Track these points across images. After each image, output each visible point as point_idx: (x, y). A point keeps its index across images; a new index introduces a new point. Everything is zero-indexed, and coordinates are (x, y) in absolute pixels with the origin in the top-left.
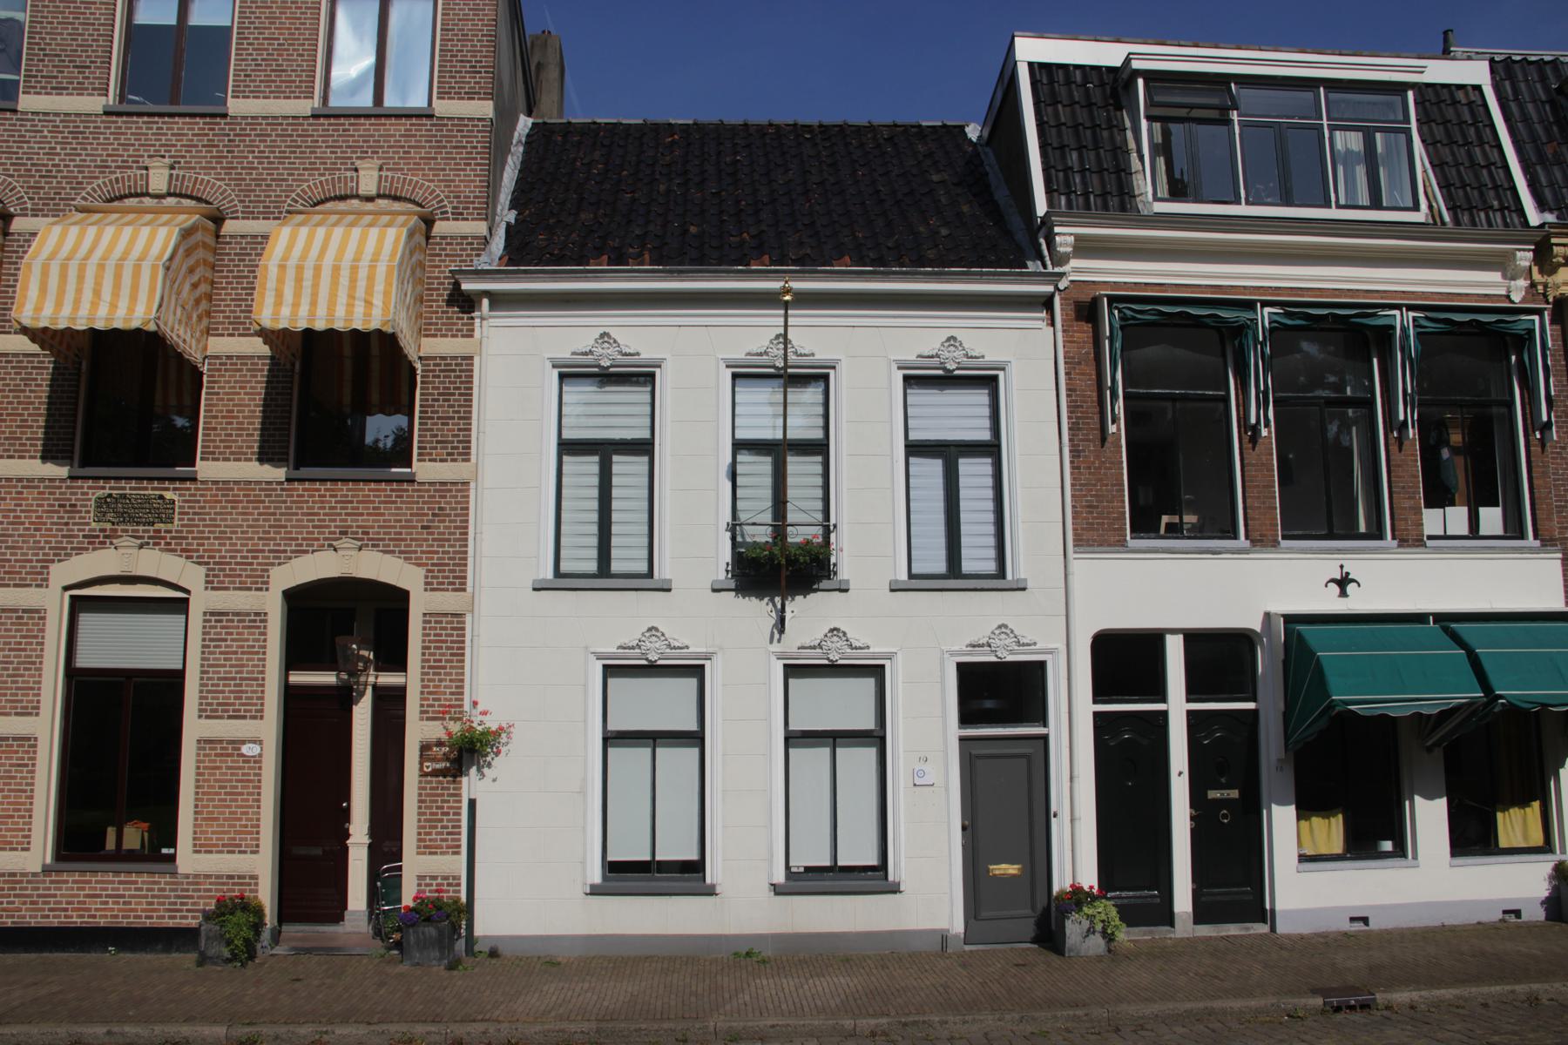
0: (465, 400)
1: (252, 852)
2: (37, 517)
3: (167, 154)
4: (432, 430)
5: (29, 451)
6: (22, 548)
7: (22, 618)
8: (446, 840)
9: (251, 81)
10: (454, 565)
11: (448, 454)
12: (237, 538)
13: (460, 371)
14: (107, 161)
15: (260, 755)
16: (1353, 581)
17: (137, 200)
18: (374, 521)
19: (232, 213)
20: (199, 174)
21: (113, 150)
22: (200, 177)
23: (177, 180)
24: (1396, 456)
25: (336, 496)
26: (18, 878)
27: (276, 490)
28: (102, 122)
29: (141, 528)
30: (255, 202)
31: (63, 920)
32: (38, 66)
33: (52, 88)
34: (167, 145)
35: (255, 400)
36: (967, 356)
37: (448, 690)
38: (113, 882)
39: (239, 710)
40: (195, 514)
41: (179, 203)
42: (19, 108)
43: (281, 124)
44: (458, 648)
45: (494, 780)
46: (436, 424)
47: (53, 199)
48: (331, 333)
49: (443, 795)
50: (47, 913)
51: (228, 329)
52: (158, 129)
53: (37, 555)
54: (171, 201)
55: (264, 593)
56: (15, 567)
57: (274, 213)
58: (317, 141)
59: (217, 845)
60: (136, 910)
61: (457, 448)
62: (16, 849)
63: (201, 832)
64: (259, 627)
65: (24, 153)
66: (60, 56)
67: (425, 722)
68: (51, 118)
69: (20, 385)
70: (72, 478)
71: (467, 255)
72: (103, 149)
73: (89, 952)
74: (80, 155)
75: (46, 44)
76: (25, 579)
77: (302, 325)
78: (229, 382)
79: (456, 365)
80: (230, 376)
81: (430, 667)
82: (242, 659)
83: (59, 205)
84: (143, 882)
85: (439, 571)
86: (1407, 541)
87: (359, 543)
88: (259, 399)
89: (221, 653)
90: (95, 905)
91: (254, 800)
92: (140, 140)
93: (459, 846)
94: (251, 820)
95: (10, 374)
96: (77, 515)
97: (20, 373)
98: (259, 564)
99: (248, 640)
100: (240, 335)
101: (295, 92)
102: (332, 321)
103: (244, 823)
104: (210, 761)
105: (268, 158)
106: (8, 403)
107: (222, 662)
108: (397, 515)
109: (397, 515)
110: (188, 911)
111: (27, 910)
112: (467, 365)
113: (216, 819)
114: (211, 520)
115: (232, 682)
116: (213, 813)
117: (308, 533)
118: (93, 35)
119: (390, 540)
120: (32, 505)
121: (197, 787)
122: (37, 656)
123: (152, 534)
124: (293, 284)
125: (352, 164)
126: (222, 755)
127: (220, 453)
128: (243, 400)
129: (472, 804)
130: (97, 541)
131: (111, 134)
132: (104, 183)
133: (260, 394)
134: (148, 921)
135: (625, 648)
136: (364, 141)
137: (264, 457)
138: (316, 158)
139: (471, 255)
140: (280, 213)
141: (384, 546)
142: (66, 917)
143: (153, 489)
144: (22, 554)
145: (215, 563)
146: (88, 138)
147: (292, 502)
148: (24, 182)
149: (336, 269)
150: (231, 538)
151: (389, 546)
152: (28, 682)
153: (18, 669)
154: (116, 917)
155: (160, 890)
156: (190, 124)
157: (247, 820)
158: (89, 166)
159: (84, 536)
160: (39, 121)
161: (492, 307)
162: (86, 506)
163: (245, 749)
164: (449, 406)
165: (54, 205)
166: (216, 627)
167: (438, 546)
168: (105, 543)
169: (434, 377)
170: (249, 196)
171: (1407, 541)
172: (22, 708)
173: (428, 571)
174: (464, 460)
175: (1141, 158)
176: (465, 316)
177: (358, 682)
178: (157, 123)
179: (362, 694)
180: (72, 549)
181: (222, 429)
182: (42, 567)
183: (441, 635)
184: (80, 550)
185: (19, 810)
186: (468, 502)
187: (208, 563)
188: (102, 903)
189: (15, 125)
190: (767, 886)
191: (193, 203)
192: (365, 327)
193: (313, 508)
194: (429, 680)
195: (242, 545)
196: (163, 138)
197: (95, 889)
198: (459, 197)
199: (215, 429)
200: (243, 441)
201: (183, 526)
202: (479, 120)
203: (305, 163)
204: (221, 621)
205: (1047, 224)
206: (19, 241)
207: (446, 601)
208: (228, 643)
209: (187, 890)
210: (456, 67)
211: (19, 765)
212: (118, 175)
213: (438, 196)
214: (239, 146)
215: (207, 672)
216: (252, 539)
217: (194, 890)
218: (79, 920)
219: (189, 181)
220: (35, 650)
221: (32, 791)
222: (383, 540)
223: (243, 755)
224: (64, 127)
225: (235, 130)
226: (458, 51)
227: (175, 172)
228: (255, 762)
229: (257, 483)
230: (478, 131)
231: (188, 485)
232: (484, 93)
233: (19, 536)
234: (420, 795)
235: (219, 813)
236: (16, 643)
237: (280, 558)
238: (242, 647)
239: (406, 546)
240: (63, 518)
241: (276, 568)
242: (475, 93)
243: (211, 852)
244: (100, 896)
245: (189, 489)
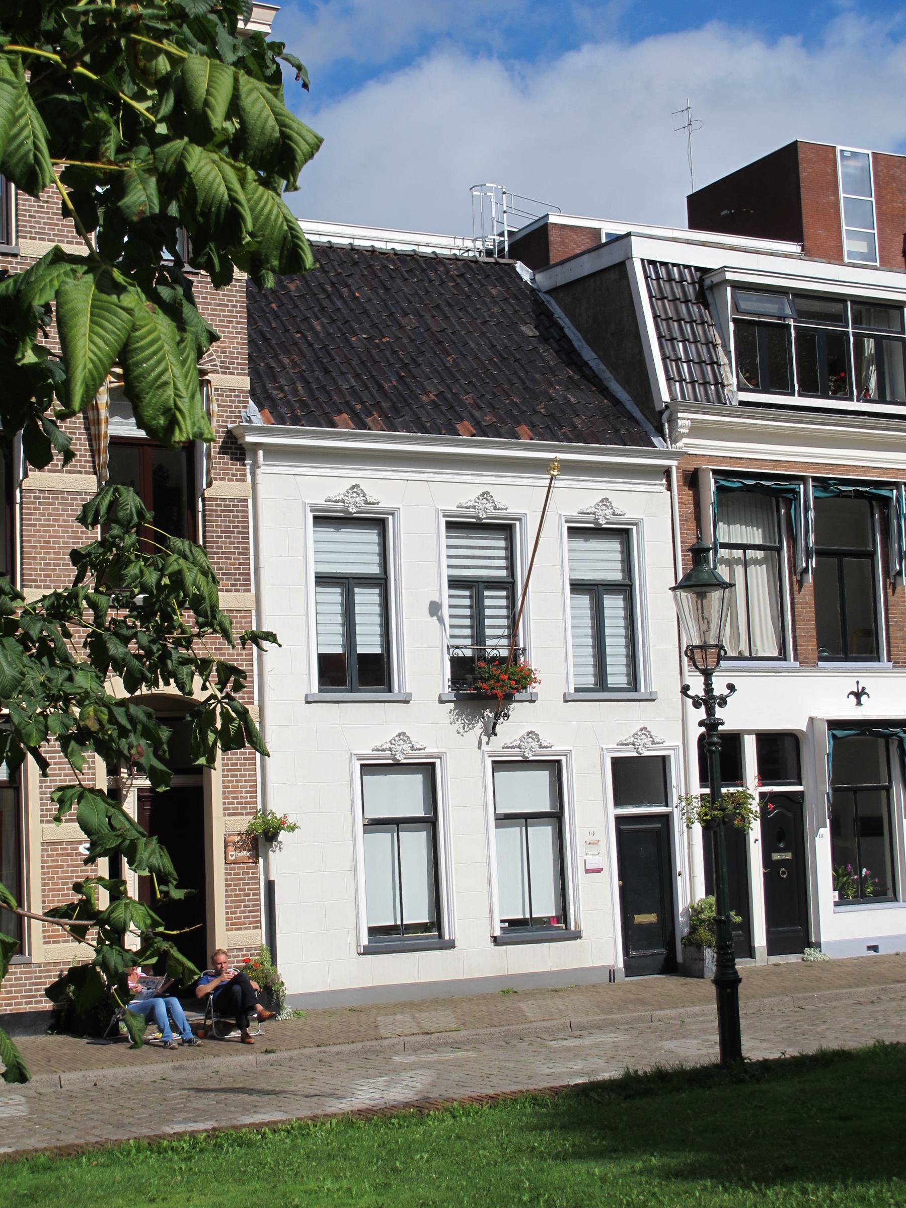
8: (248, 917)
11: (232, 585)
16: (866, 693)
24: (890, 598)
36: (366, 502)
46: (221, 558)
61: (239, 580)
67: (227, 818)
71: (236, 407)
78: (44, 515)
81: (229, 770)
86: (898, 663)
104: (53, 861)
126: (62, 855)
127: (41, 581)
128: (58, 531)
129: (270, 886)
139: (238, 407)
164: (231, 543)
169: (217, 516)
171: (898, 663)
175: (728, 354)
181: (41, 559)
190: (489, 939)
199: (35, 558)
200: (60, 570)
205: (671, 409)
209: (40, 978)
243: (58, 942)
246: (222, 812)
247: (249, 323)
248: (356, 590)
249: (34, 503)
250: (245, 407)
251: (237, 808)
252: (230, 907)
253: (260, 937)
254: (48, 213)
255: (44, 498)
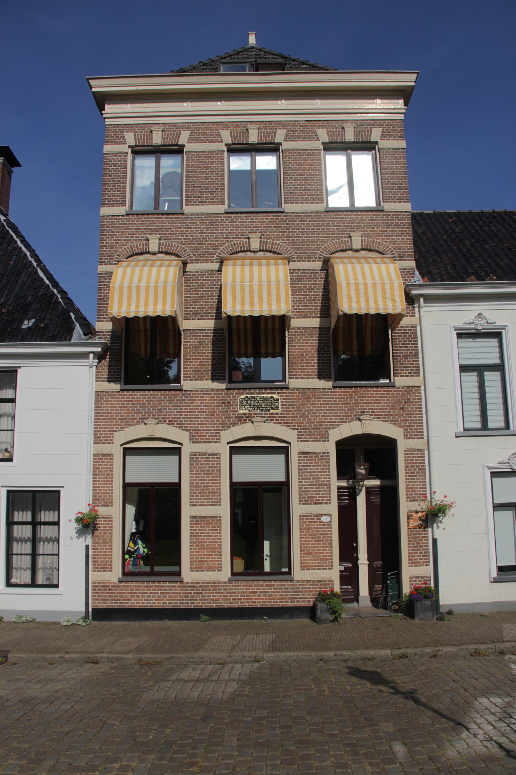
0: (415, 347)
1: (329, 569)
2: (212, 409)
3: (257, 231)
4: (400, 361)
5: (205, 377)
6: (205, 424)
7: (209, 458)
8: (422, 559)
9: (293, 195)
10: (417, 426)
11: (409, 373)
12: (311, 416)
13: (411, 333)
14: (228, 235)
15: (331, 522)
17: (244, 253)
18: (377, 406)
19: (292, 258)
20: (274, 240)
21: (231, 230)
22: (275, 242)
23: (263, 243)
25: (357, 394)
26: (217, 584)
27: (328, 392)
28: (224, 217)
29: (263, 412)
30: (302, 253)
31: (240, 604)
32: (192, 192)
33: (199, 202)
34: (257, 227)
35: (313, 349)
36: (487, 323)
37: (419, 487)
38: (263, 586)
39: (319, 500)
40: (289, 405)
41: (264, 254)
42: (185, 213)
43: (311, 216)
44: (422, 466)
45: (444, 529)
46: (402, 359)
47: (205, 254)
48: (136, 318)
49: (419, 537)
50: (232, 601)
51: (297, 315)
52: (251, 219)
53: (213, 427)
54: (261, 254)
55: (326, 442)
56: (203, 433)
57: (312, 258)
58: (329, 224)
59: (312, 566)
60: (274, 599)
61: (413, 370)
62: (215, 571)
63: (304, 560)
64: (325, 459)
65: (189, 233)
66: (201, 187)
67: (409, 503)
68: (200, 216)
69: (198, 345)
70: (121, 390)
71: (408, 277)
72: (226, 230)
73: (254, 619)
74: (215, 233)
75: (194, 182)
76: (209, 439)
77: (123, 315)
78: (300, 340)
79: (409, 330)
80: (300, 338)
81: (409, 476)
82: (318, 475)
83: (208, 257)
84: (277, 585)
85: (410, 429)
87: (157, 421)
88: (315, 348)
89: (308, 472)
90: (254, 597)
91: (329, 544)
92: (243, 225)
93: (429, 562)
94: (328, 553)
95: (192, 339)
96: (231, 407)
97: (197, 339)
98: (323, 428)
99: (320, 466)
100: (303, 318)
101: (315, 200)
102: (378, 309)
103: (324, 555)
104: (306, 525)
105: (306, 232)
106: (193, 353)
107: (309, 477)
108: (387, 403)
109: (387, 403)
110: (300, 598)
111: (222, 599)
112: (414, 330)
113: (311, 553)
114: (297, 407)
115: (314, 487)
116: (309, 550)
117: (345, 413)
118: (216, 176)
119: (385, 415)
120: (209, 403)
121: (301, 538)
122: (217, 477)
123: (269, 415)
124: (355, 292)
125: (146, 237)
126: (312, 522)
127: (299, 375)
129: (435, 541)
130: (248, 418)
131: (229, 222)
132: (228, 246)
133: (315, 346)
134: (281, 604)
135: (501, 463)
136: (352, 223)
137: (320, 376)
138: (329, 231)
139: (409, 277)
140: (316, 258)
141: (383, 418)
142: (241, 603)
143: (268, 393)
144: (206, 427)
145: (301, 429)
146: (218, 225)
147: (336, 398)
148: (190, 247)
149: (147, 287)
150: (308, 416)
151: (385, 418)
152: (214, 489)
153: (209, 483)
154: (265, 602)
155: (285, 589)
156: (266, 216)
157: (326, 553)
158: (220, 238)
159: (236, 417)
160: (195, 218)
161: (425, 301)
162: (235, 402)
163: (323, 519)
164: (407, 350)
165: (205, 257)
166: (304, 460)
167: (408, 417)
168: (246, 420)
169: (399, 336)
170: (300, 250)
172: (212, 502)
173: (405, 429)
174: (417, 376)
176: (410, 306)
177: (359, 484)
178: (251, 216)
179: (360, 491)
180: (230, 424)
182: (216, 433)
183: (413, 460)
184: (234, 424)
185: (215, 552)
186: (421, 396)
187: (298, 429)
188: (258, 596)
189: (184, 220)
191: (271, 254)
192: (394, 312)
193: (347, 401)
194: (409, 482)
195: (314, 419)
196: (255, 224)
197: (254, 589)
198: (400, 249)
199: (295, 363)
201: (284, 411)
202: (405, 212)
203: (324, 234)
204: (306, 457)
206: (190, 275)
207: (416, 444)
208: (311, 467)
209: (299, 588)
210: (390, 187)
211: (213, 530)
212: (235, 242)
213: (390, 249)
214: (291, 226)
215: (302, 482)
216: (318, 416)
217: (302, 588)
218: (247, 604)
219: (269, 244)
220: (216, 474)
221: (220, 542)
222: (382, 415)
223: (322, 522)
224: (206, 220)
225: (289, 219)
226: (391, 179)
227: (262, 240)
228: (328, 525)
229: (318, 389)
230: (406, 218)
231: (284, 391)
232: (406, 199)
233: (204, 418)
234: (409, 538)
235: (312, 550)
236: (207, 471)
237: (333, 425)
238: (318, 469)
239: (393, 418)
240: (224, 409)
241: (117, 433)
242: (402, 199)
243: (309, 569)
244: (257, 592)
245: (285, 393)
246: (405, 499)
247: (413, 233)
248: (485, 373)
249: (295, 335)
250: (413, 277)
251: (415, 497)
252: (411, 553)
253: (429, 570)
254: (300, 190)
255: (300, 332)
